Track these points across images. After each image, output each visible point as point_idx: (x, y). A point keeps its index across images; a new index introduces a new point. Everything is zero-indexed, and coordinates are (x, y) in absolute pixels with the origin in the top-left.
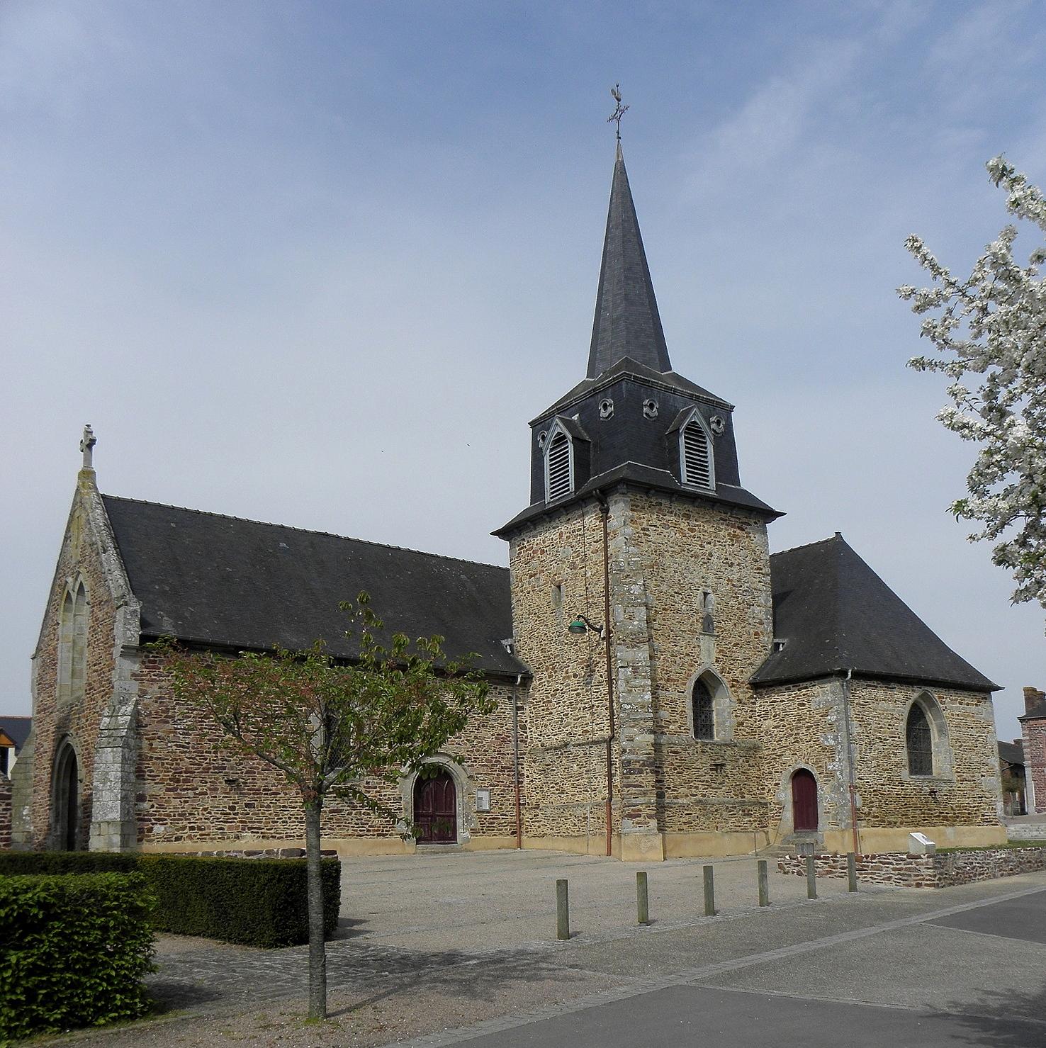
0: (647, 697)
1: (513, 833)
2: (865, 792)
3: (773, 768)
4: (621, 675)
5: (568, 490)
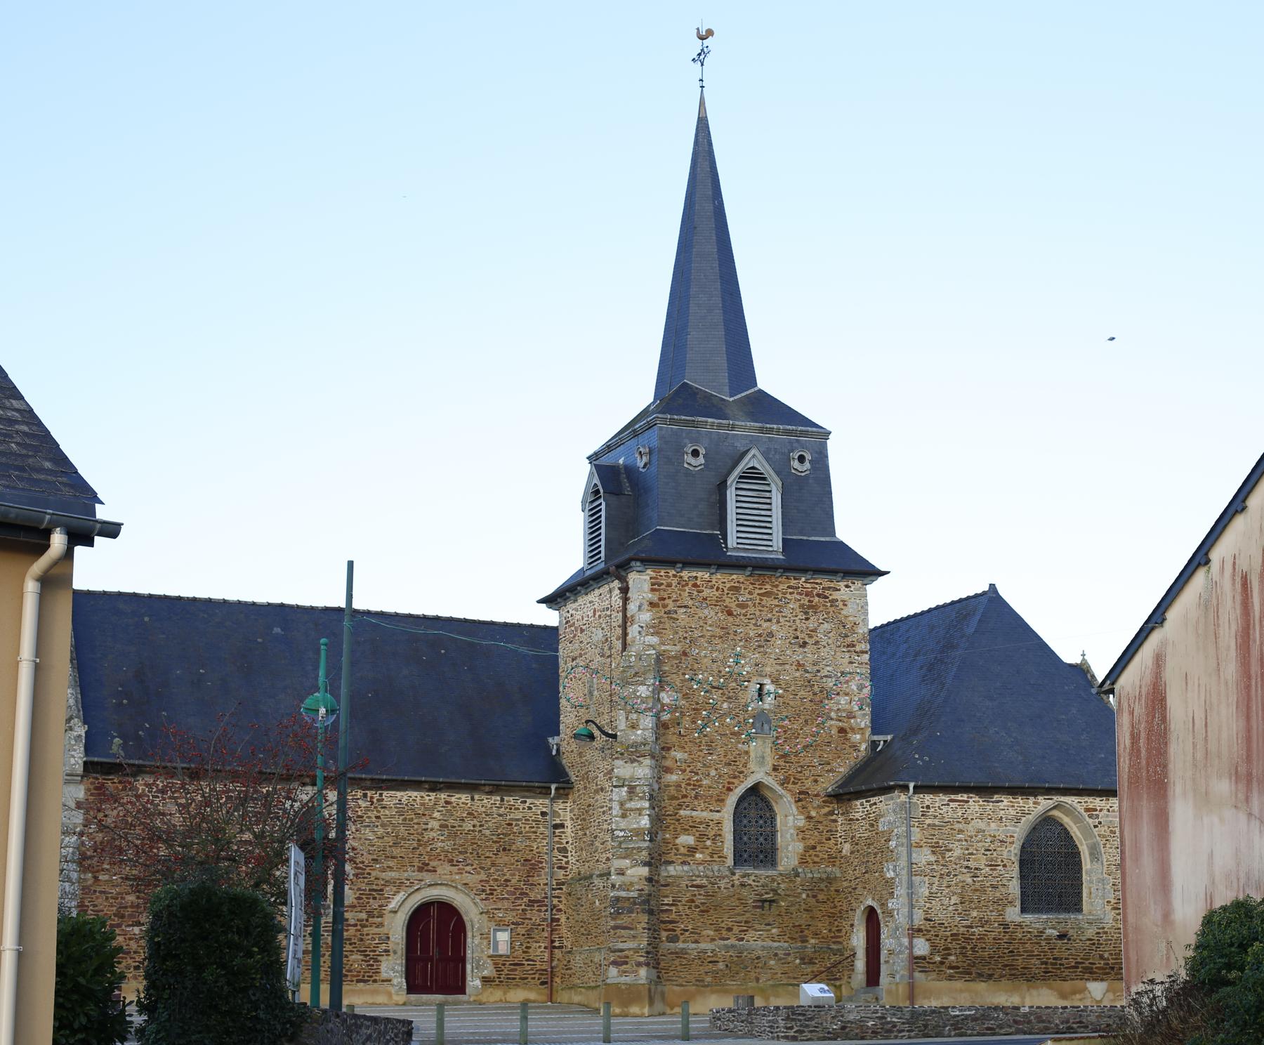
0: (643, 822)
1: (542, 983)
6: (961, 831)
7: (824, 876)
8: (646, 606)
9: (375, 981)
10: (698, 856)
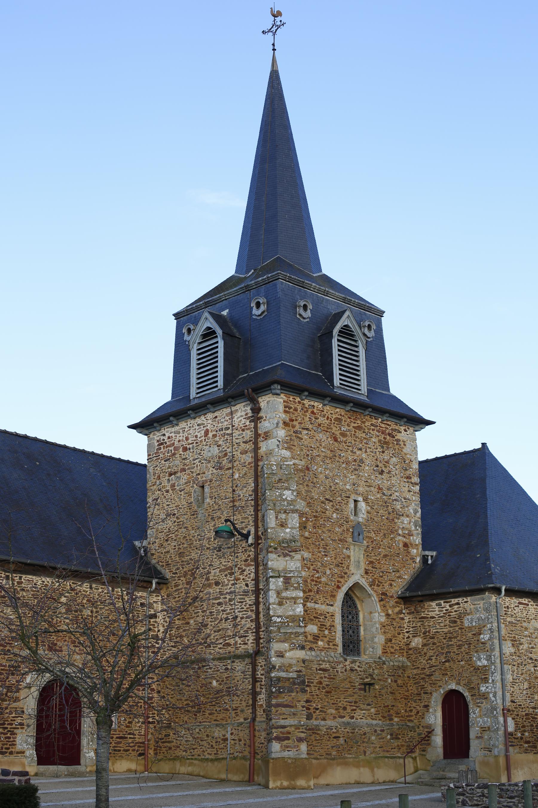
1: (140, 755)
2: (518, 715)
3: (422, 688)
4: (272, 586)
5: (217, 386)
6: (526, 629)
7: (400, 664)
8: (281, 424)
9: (11, 753)
10: (320, 643)
